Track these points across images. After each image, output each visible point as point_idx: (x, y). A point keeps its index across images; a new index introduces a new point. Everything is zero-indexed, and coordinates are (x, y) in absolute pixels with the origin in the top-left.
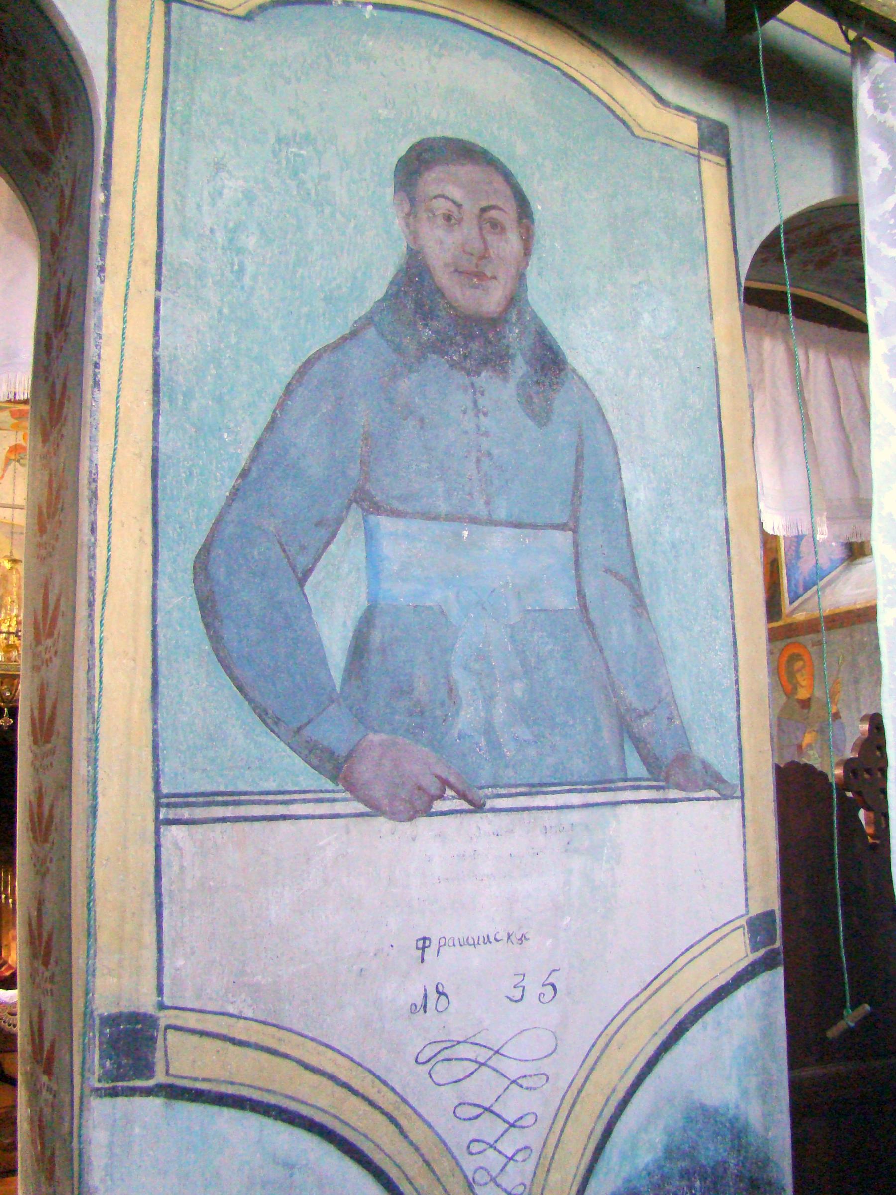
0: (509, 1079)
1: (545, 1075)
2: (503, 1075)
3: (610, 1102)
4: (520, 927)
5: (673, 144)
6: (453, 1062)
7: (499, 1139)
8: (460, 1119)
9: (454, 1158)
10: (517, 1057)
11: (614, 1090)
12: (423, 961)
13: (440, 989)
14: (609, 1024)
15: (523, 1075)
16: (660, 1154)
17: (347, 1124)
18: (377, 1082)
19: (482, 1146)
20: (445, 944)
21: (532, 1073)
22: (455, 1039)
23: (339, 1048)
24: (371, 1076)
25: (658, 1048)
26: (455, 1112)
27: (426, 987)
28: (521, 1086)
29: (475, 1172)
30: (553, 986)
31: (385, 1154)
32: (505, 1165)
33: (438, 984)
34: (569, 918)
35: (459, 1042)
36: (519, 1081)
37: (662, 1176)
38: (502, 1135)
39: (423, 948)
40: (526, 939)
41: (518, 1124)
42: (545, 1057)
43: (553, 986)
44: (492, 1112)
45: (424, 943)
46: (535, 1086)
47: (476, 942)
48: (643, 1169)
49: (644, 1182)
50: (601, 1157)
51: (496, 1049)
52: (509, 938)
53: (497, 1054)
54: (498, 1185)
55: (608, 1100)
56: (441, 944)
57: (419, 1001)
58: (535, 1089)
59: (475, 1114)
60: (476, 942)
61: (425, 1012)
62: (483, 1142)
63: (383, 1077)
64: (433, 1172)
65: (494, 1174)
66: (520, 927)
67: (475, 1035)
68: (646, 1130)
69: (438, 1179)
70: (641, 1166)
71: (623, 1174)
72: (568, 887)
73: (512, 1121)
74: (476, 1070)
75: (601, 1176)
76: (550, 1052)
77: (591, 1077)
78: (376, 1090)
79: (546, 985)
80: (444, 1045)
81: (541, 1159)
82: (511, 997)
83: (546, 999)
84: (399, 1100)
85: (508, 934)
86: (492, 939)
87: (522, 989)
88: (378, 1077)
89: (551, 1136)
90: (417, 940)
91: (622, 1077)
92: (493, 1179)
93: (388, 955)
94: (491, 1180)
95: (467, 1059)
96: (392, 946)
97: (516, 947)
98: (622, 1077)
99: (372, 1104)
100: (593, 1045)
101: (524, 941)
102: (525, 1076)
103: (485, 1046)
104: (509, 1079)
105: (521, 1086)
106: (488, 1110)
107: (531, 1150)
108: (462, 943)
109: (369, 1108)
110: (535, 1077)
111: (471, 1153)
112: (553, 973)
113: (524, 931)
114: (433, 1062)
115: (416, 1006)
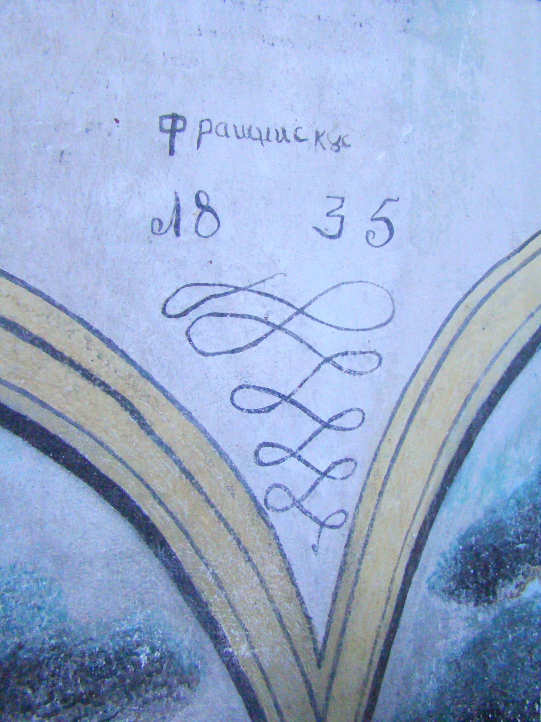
0: (321, 355)
1: (378, 355)
2: (310, 347)
3: (470, 404)
4: (336, 127)
5: (343, 596)
6: (228, 319)
7: (305, 444)
8: (242, 409)
9: (233, 468)
10: (335, 324)
11: (475, 387)
12: (172, 152)
13: (204, 200)
14: (469, 292)
15: (343, 351)
16: (534, 478)
17: (44, 405)
18: (96, 340)
19: (278, 454)
20: (210, 132)
21: (357, 350)
22: (229, 283)
23: (24, 278)
24: (85, 331)
25: (535, 336)
26: (232, 399)
27: (179, 195)
28: (340, 368)
29: (268, 492)
30: (387, 221)
31: (115, 456)
32: (316, 483)
33: (200, 191)
34: (411, 128)
35: (237, 289)
36: (337, 360)
37: (535, 506)
38: (310, 439)
39: (173, 132)
40: (344, 144)
41: (334, 423)
42: (377, 327)
43: (387, 221)
44: (293, 402)
45: (174, 123)
46: (359, 369)
47: (264, 137)
48: (511, 498)
49: (511, 513)
50: (456, 478)
51: (299, 307)
52: (318, 138)
53: (301, 315)
54: (305, 512)
55: (468, 398)
56: (204, 130)
57: (167, 217)
58: (361, 374)
59: (266, 405)
60: (264, 137)
61: (177, 234)
62: (280, 447)
63: (106, 333)
64: (200, 489)
65: (298, 497)
66: (336, 127)
67: (263, 281)
68: (517, 445)
69: (208, 500)
70: (509, 493)
71: (486, 502)
72: (409, 83)
73: (326, 420)
74: (266, 335)
75: (456, 504)
76: (384, 321)
77: (445, 365)
78: (94, 354)
79: (377, 219)
80: (211, 291)
81: (371, 477)
82: (322, 229)
83: (376, 241)
84: (136, 373)
85: (317, 133)
86: (290, 136)
87: (339, 219)
88: (97, 333)
89: (385, 444)
90: (161, 118)
91: (487, 370)
92: (297, 503)
93: (110, 135)
94: (294, 504)
95: (250, 317)
96: (117, 121)
97: (330, 155)
98: (487, 370)
99: (88, 375)
100: (448, 319)
101: (342, 149)
102: (346, 353)
103: (281, 300)
104: (321, 355)
105: (340, 368)
106: (287, 399)
107: (356, 464)
108: (241, 135)
109: (83, 382)
110: (362, 356)
111: (261, 464)
112: (388, 204)
113: (343, 132)
114: (193, 315)
115: (161, 223)
